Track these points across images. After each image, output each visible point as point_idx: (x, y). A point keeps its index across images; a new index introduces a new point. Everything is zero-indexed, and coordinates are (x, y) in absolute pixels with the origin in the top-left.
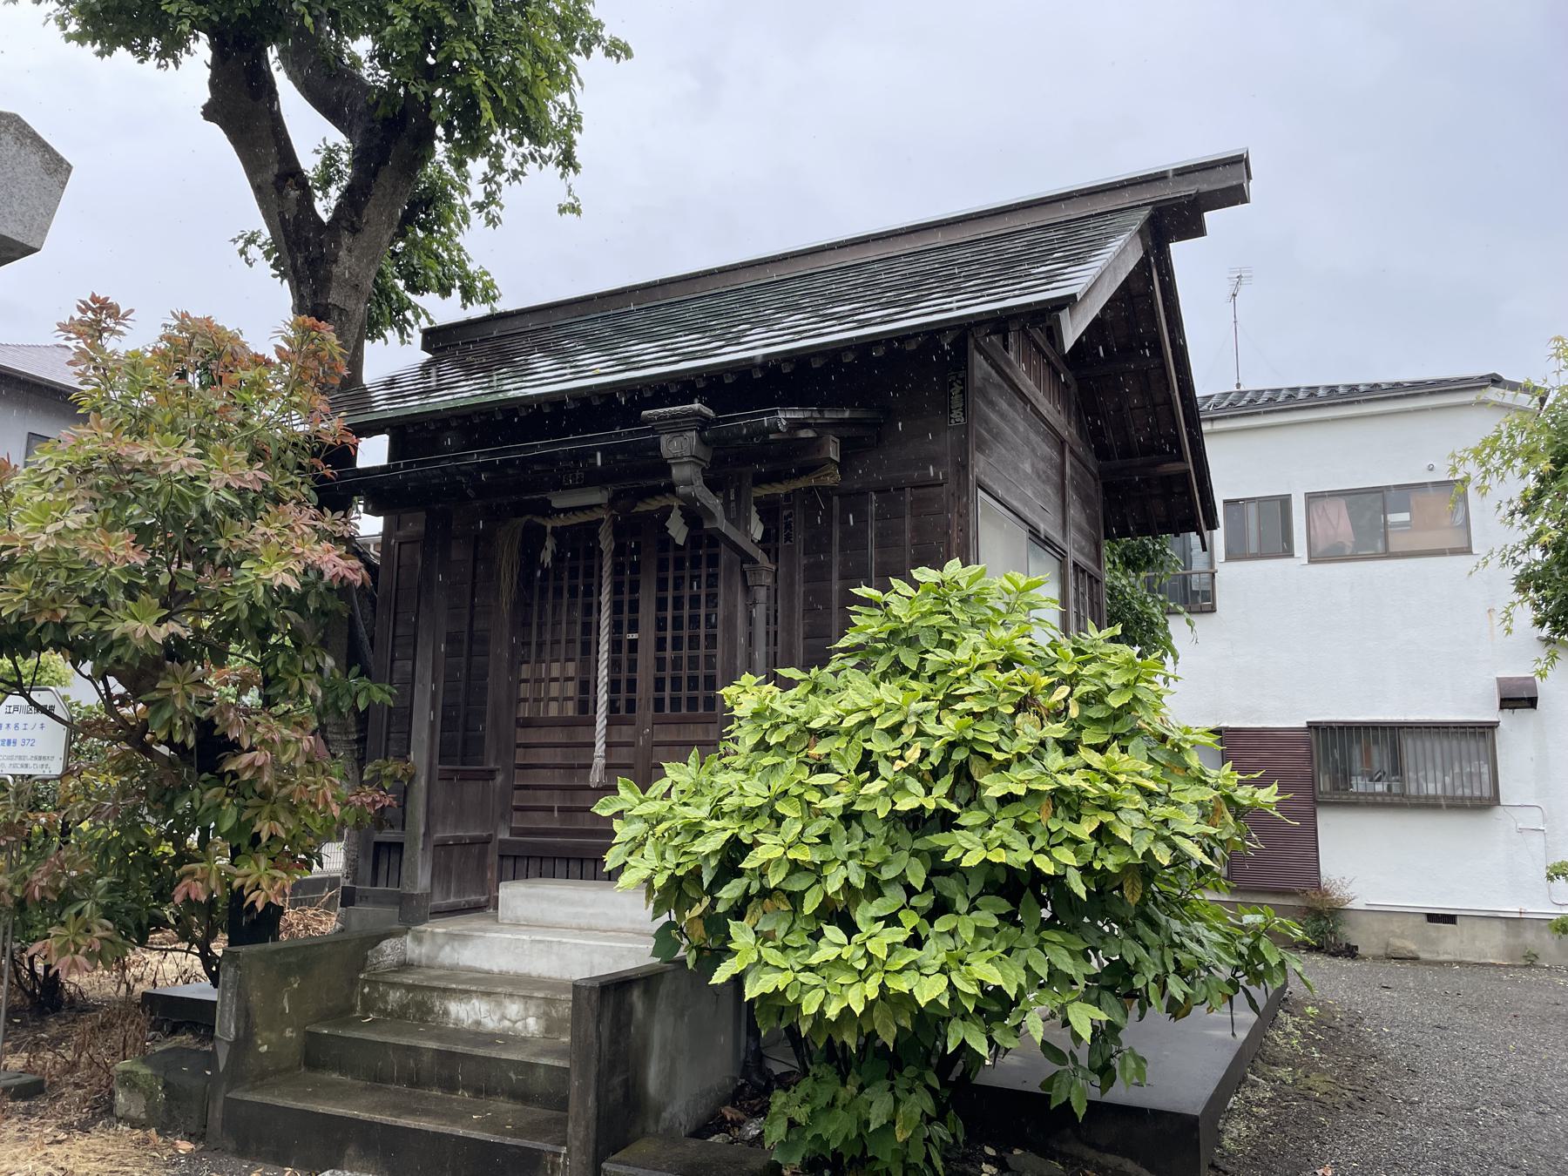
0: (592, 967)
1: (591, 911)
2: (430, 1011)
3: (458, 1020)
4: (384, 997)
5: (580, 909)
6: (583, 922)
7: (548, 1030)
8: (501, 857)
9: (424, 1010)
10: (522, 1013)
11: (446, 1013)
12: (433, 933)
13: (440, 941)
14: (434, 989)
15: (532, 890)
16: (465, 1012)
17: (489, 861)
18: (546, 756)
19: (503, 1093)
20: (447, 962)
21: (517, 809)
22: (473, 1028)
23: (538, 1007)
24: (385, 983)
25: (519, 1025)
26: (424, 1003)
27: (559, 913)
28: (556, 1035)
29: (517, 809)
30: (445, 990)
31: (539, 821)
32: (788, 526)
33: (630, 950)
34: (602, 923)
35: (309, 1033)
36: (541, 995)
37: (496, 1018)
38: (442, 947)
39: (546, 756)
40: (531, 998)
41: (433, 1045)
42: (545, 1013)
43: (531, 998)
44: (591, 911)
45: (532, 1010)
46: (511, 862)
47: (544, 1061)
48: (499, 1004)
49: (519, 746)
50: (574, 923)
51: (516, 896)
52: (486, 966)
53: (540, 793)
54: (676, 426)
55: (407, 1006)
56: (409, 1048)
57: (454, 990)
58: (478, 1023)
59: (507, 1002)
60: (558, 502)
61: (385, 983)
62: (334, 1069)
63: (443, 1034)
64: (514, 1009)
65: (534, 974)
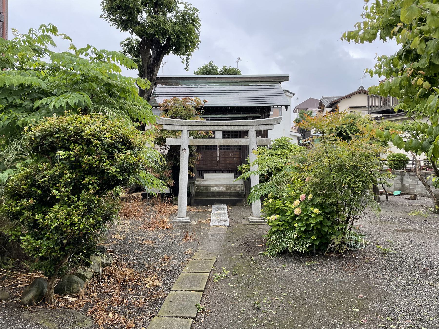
4: (200, 188)
7: (227, 189)
9: (207, 189)
16: (213, 189)
27: (215, 177)
64: (221, 188)
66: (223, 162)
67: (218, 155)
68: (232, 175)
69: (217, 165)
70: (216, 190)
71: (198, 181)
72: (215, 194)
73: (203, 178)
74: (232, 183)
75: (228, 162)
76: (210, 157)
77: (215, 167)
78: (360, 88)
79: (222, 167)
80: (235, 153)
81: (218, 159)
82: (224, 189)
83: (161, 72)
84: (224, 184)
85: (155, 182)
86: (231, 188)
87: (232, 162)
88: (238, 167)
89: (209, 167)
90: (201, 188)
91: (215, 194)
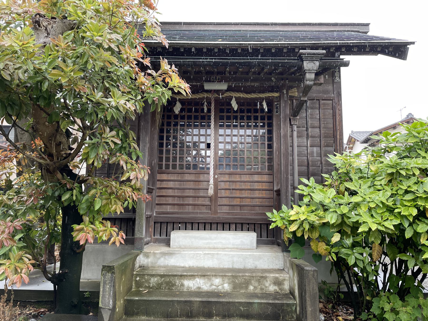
0: (233, 263)
1: (215, 241)
2: (174, 285)
3: (188, 287)
4: (148, 281)
5: (210, 241)
6: (211, 246)
7: (234, 288)
8: (155, 223)
9: (170, 285)
10: (221, 282)
11: (182, 285)
12: (154, 254)
13: (158, 256)
14: (176, 276)
15: (187, 234)
16: (191, 284)
17: (151, 225)
18: (171, 184)
19: (237, 316)
20: (162, 264)
21: (157, 204)
22: (197, 290)
23: (229, 279)
24: (148, 275)
25: (220, 287)
26: (170, 282)
27: (201, 243)
28: (238, 290)
29: (157, 204)
30: (181, 276)
31: (169, 209)
32: (277, 108)
33: (250, 255)
34: (220, 246)
35: (127, 300)
36: (230, 274)
37: (208, 285)
38: (159, 258)
39: (171, 184)
40: (225, 276)
41: (198, 299)
42: (233, 282)
43: (225, 276)
44: (215, 241)
45: (226, 281)
46: (159, 225)
47: (257, 301)
48: (210, 280)
49: (158, 180)
50: (207, 246)
51: (178, 237)
52: (182, 265)
53: (167, 198)
54: (312, 57)
55: (162, 284)
56: (186, 302)
57: (186, 276)
58: (199, 288)
59: (213, 278)
60: (207, 86)
61: (148, 275)
62: (143, 314)
63: (182, 293)
64: (217, 281)
65: (206, 266)
66: (225, 201)
67: (212, 181)
68: (249, 238)
69: (208, 207)
70: (199, 293)
71: (147, 255)
72: (195, 307)
73: (168, 243)
74: (250, 264)
75: (237, 202)
76: (191, 185)
77: (204, 214)
78: (408, 116)
79: (223, 212)
80: (256, 178)
81: (211, 192)
82: (227, 287)
83: (204, 155)
84: (226, 264)
85: (369, 199)
86: (247, 283)
87: (247, 202)
88: (269, 214)
89: (189, 212)
90: (154, 281)
91: (195, 307)
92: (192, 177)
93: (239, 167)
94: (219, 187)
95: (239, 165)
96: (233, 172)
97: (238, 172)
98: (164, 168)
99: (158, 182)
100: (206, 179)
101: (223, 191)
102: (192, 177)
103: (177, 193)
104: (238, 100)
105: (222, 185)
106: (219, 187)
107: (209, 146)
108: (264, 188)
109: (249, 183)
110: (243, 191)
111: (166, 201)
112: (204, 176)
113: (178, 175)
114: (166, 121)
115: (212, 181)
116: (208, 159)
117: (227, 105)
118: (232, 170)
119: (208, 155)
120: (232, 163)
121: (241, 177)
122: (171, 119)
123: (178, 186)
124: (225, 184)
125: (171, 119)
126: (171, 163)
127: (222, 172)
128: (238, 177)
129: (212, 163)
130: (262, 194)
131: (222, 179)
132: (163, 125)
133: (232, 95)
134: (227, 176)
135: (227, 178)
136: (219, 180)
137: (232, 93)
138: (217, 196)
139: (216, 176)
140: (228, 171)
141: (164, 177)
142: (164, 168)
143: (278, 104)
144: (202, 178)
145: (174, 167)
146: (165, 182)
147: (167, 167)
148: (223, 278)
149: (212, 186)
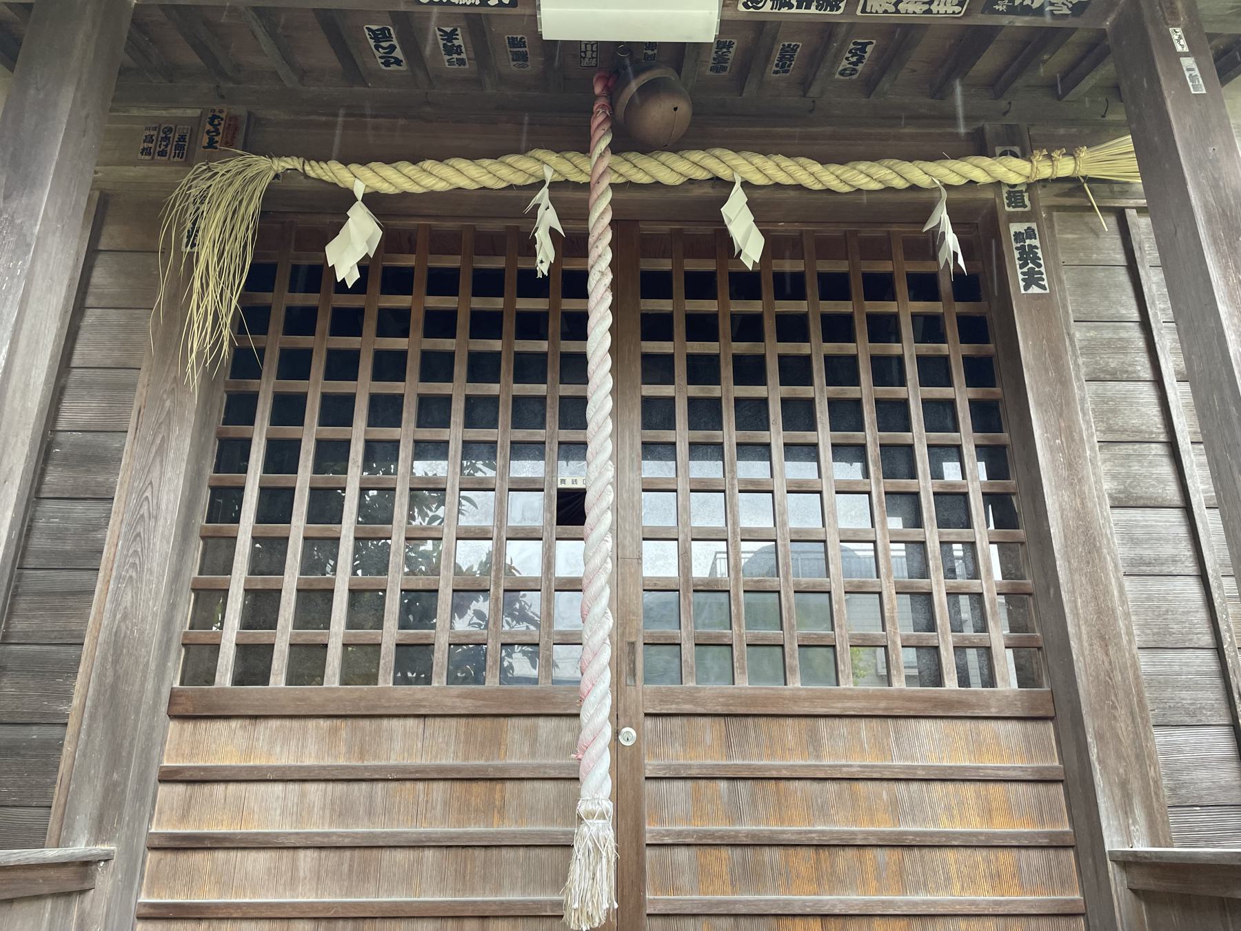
18: (269, 810)
92: (440, 747)
93: (794, 657)
94: (652, 829)
95: (792, 648)
96: (754, 700)
97: (795, 699)
98: (224, 676)
99: (163, 790)
100: (552, 761)
101: (682, 855)
102: (440, 747)
103: (312, 811)
104: (763, 204)
105: (673, 814)
106: (652, 829)
107: (571, 508)
108: (1000, 827)
109: (884, 789)
110: (844, 858)
111: (223, 884)
112: (533, 737)
113: (334, 732)
114: (275, 342)
115: (597, 790)
116: (565, 661)
117: (695, 248)
118: (743, 682)
119: (563, 570)
120: (739, 633)
121: (814, 743)
122: (306, 377)
123: (318, 826)
124: (697, 799)
125: (312, 332)
126: (284, 635)
127: (664, 698)
128: (790, 739)
129: (601, 628)
130: (996, 878)
131: (675, 756)
132: (245, 364)
133: (724, 173)
134: (709, 731)
135: (706, 748)
136: (651, 765)
137: (728, 155)
138: (640, 902)
139: (629, 735)
140: (713, 691)
141: (224, 745)
142: (224, 676)
143: (1030, 234)
144: (518, 747)
145: (307, 661)
146: (219, 789)
147: (253, 665)
148: (611, 484)
149: (597, 832)
